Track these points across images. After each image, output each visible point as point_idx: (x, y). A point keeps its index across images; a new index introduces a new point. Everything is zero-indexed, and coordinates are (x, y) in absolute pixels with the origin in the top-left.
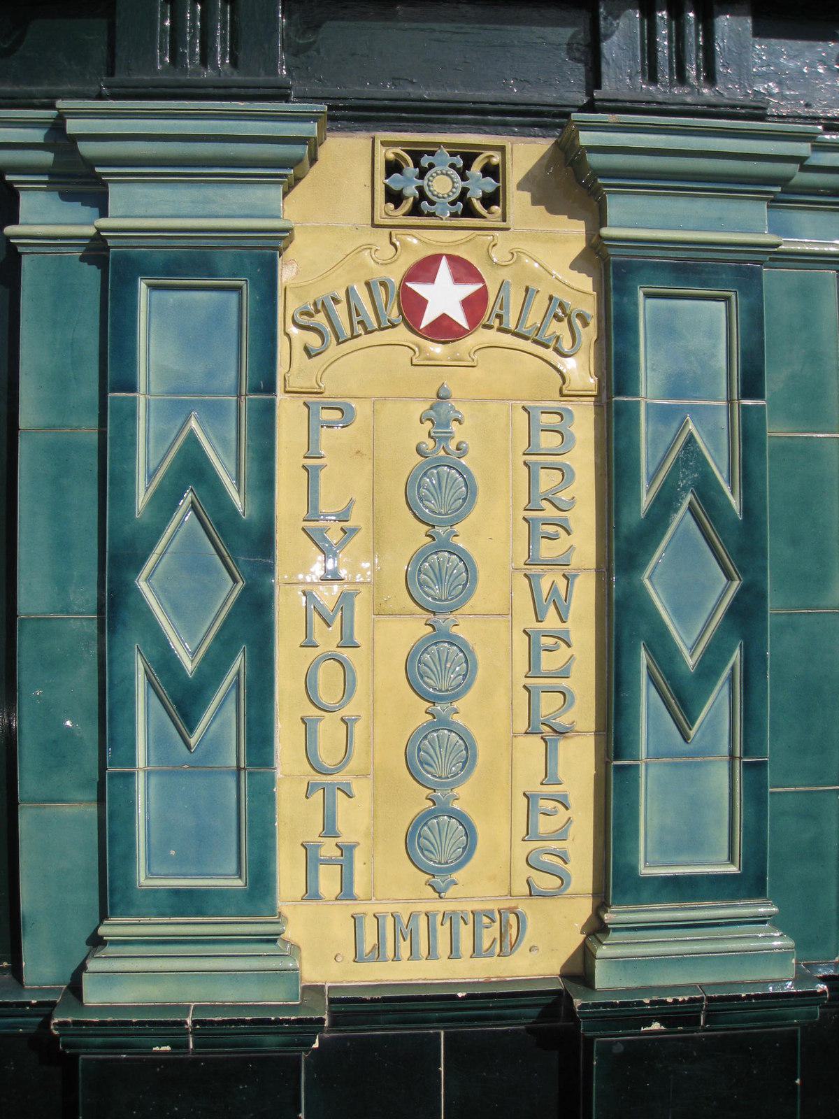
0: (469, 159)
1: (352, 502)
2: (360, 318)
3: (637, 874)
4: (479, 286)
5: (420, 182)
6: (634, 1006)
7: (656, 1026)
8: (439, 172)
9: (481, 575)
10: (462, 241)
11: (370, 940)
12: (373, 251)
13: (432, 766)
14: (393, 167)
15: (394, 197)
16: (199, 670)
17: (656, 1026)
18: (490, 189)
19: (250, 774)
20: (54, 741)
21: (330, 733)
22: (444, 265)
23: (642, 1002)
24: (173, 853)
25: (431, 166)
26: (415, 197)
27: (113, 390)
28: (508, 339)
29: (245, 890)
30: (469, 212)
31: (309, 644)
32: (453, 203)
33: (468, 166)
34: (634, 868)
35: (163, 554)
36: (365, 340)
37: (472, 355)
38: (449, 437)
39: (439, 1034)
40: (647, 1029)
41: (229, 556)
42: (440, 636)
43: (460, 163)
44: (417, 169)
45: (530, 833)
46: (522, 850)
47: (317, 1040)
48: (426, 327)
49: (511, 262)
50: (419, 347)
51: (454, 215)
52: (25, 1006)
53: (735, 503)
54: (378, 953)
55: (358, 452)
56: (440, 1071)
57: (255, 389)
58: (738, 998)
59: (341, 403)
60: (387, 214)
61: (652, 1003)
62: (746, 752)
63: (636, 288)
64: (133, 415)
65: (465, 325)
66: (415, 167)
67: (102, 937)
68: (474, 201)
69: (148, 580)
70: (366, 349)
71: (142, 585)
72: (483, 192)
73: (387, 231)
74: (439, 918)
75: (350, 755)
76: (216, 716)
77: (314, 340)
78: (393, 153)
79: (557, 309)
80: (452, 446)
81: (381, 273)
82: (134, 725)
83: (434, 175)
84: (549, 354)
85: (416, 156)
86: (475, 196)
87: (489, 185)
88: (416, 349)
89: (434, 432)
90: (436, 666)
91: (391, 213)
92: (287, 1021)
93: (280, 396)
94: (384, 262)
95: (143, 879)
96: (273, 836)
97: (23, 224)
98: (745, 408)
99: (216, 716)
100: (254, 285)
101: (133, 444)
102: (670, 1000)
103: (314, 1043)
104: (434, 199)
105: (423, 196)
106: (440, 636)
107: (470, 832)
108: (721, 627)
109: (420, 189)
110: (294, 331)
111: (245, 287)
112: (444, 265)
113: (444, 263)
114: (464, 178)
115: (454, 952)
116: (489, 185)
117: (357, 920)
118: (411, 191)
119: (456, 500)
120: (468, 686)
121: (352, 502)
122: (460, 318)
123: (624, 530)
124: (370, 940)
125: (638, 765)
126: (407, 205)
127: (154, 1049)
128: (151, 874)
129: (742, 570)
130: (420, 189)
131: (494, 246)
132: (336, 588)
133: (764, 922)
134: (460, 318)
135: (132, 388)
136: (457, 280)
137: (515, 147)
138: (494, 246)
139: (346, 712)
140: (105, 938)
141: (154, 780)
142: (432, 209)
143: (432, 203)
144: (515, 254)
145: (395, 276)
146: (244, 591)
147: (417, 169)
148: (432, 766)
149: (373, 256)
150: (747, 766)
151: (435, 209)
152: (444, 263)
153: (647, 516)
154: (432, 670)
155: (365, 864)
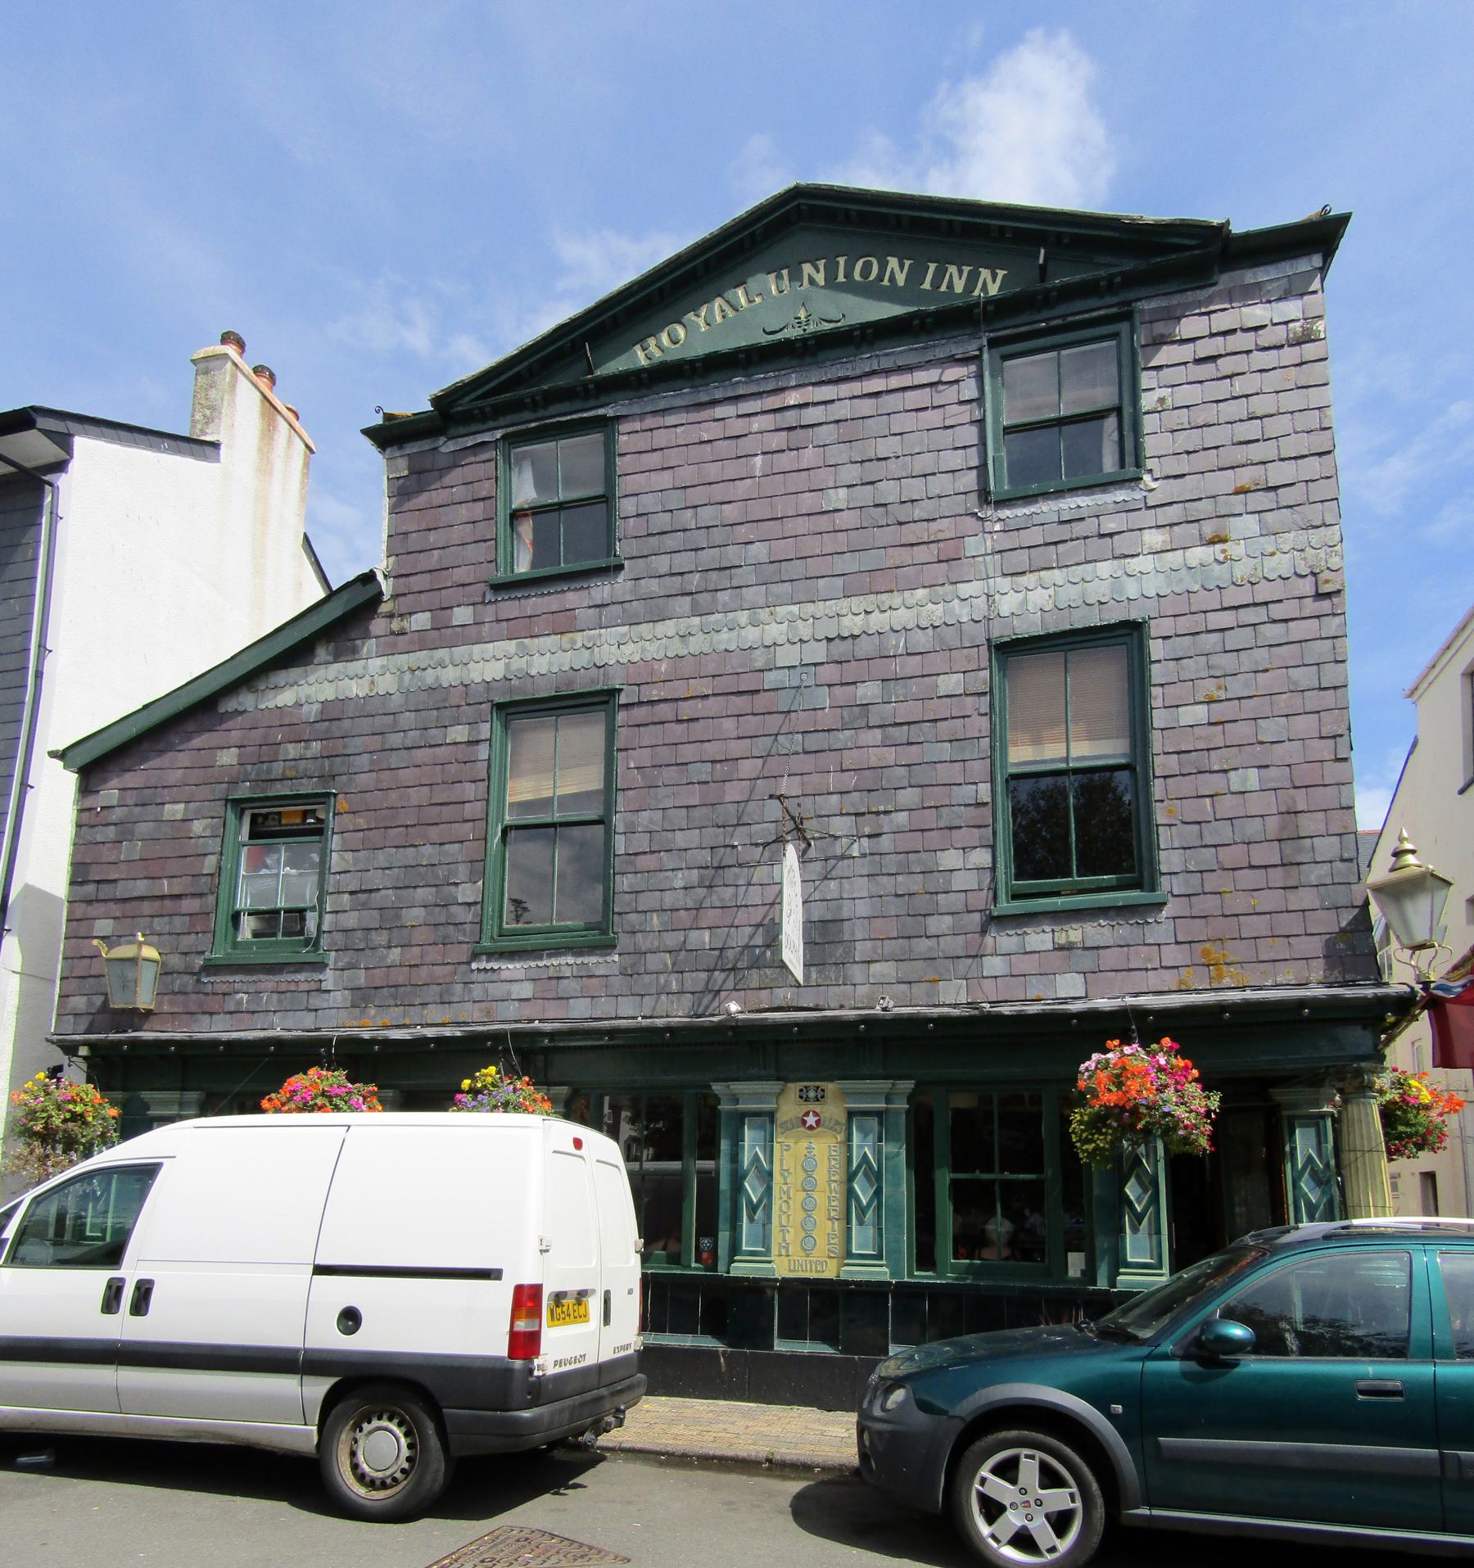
0: (818, 1088)
14: (801, 1090)
15: (801, 1097)
21: (784, 1217)
30: (818, 1100)
31: (781, 1198)
46: (827, 1247)
54: (794, 1271)
71: (746, 1184)
79: (837, 1123)
95: (744, 1248)
115: (811, 1271)
117: (790, 1261)
122: (814, 1125)
134: (814, 1125)
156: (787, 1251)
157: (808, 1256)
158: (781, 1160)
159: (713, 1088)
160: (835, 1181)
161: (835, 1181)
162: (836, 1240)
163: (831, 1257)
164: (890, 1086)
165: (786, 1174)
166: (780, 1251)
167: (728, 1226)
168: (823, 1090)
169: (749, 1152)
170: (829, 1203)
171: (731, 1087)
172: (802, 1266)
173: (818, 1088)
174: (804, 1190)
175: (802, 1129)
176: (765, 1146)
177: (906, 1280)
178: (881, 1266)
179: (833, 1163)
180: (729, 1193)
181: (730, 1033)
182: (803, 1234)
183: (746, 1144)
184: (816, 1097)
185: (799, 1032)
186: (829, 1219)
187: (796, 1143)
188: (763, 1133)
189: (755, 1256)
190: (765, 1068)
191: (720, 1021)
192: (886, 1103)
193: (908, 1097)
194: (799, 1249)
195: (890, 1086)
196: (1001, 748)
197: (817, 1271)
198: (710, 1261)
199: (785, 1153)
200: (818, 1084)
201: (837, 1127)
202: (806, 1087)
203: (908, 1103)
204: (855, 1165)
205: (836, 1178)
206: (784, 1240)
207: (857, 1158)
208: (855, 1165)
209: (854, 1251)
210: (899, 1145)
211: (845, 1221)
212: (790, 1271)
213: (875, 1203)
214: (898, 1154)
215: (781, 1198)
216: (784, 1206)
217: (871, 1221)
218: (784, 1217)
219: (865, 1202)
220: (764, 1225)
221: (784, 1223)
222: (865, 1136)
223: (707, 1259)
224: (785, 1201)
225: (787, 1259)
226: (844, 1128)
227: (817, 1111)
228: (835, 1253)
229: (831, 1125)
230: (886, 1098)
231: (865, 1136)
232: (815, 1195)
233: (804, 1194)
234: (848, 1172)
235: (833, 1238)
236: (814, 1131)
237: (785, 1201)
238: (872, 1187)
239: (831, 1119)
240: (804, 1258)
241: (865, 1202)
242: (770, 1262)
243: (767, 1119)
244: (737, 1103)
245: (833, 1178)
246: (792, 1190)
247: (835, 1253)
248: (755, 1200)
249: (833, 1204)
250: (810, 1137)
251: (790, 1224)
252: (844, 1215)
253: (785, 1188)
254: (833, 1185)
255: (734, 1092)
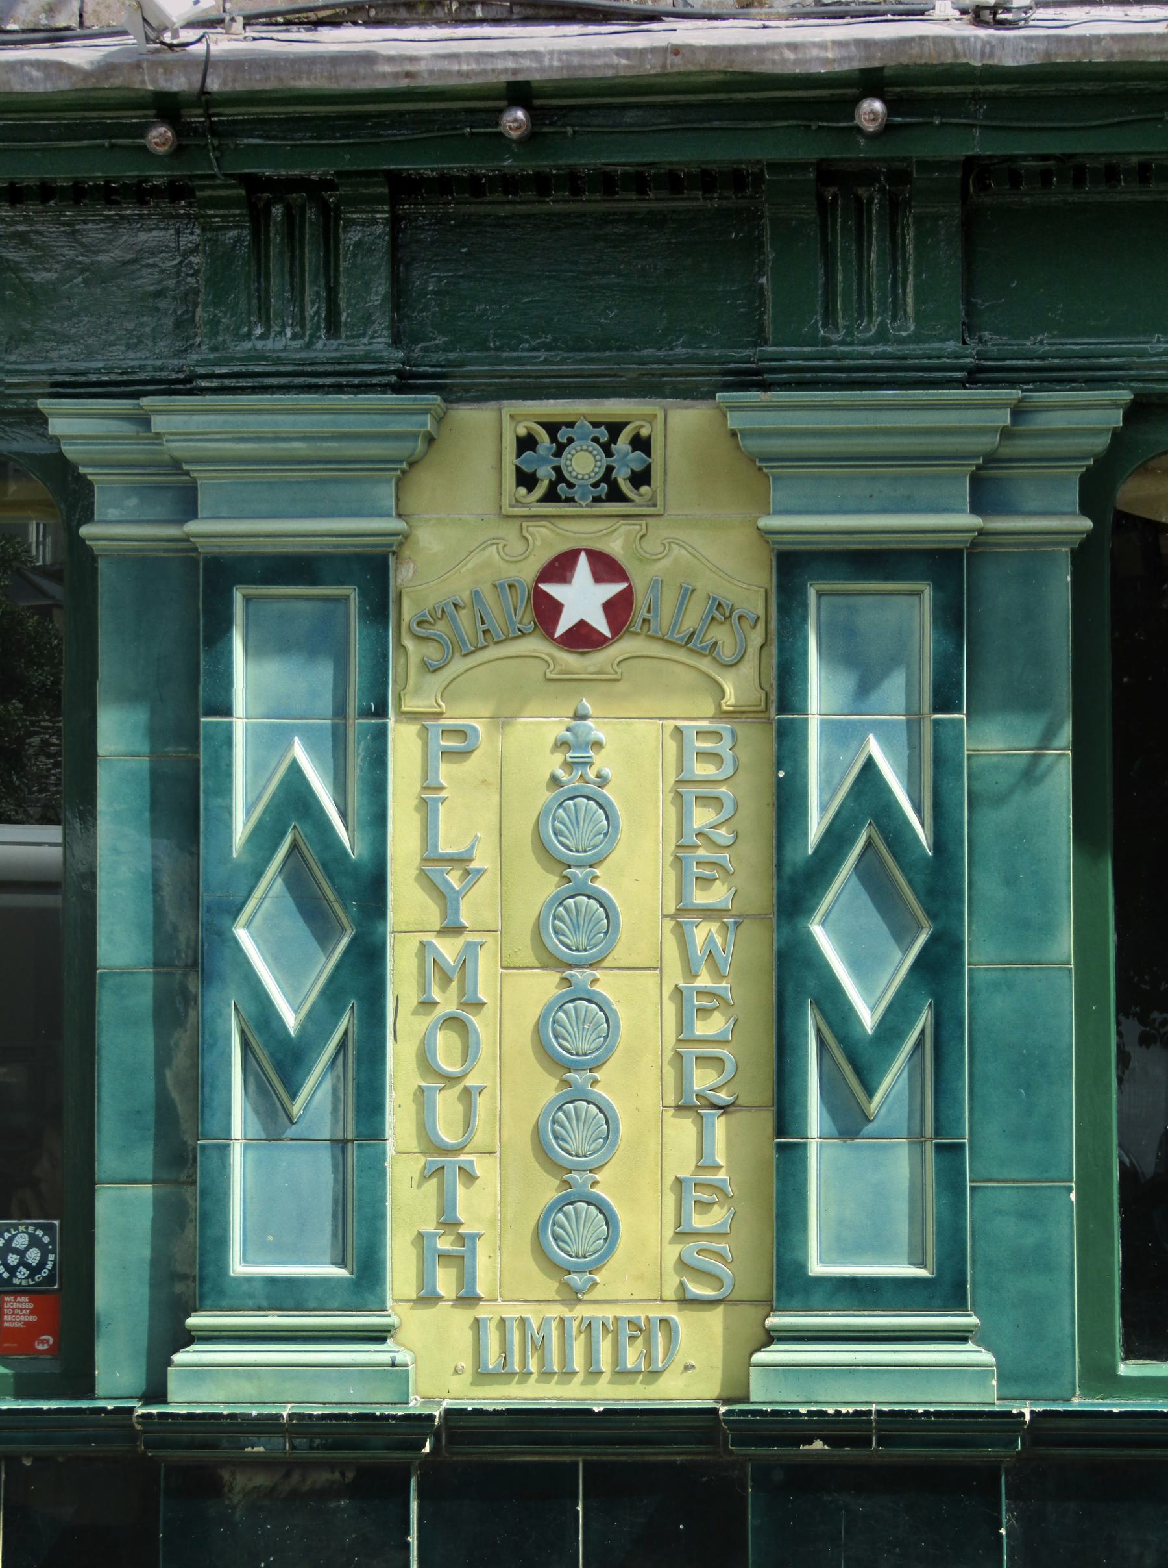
0: (615, 429)
1: (476, 839)
2: (485, 627)
3: (806, 1273)
4: (624, 585)
5: (556, 461)
6: (788, 1416)
7: (818, 1445)
8: (579, 448)
9: (624, 919)
10: (604, 532)
11: (493, 1358)
12: (500, 546)
13: (568, 1143)
14: (526, 444)
15: (526, 480)
16: (303, 1028)
17: (818, 1445)
18: (638, 468)
19: (359, 1146)
20: (138, 1112)
21: (446, 1104)
22: (583, 561)
23: (798, 1411)
24: (270, 1238)
25: (571, 440)
26: (550, 480)
27: (207, 714)
28: (656, 649)
29: (352, 1279)
30: (616, 495)
31: (427, 1005)
32: (596, 485)
33: (614, 439)
34: (802, 1267)
35: (262, 900)
36: (493, 652)
37: (615, 666)
38: (586, 763)
39: (576, 1464)
40: (807, 1447)
41: (328, 901)
42: (575, 994)
43: (605, 438)
44: (554, 445)
45: (682, 1234)
46: (672, 1252)
47: (428, 1444)
48: (562, 636)
49: (664, 554)
50: (553, 658)
51: (597, 499)
52: (942, 124)
53: (922, 834)
54: (504, 1375)
55: (484, 782)
56: (578, 1511)
57: (365, 713)
58: (914, 1413)
59: (464, 725)
60: (517, 501)
61: (810, 1413)
62: (937, 1133)
63: (806, 585)
64: (229, 742)
65: (607, 633)
66: (552, 442)
67: (190, 1331)
68: (620, 481)
69: (823, 923)
70: (493, 663)
71: (242, 935)
72: (649, 437)
73: (518, 522)
74: (575, 1324)
75: (473, 1128)
76: (321, 1082)
77: (432, 652)
78: (526, 427)
79: (720, 612)
80: (591, 774)
81: (511, 572)
82: (230, 1091)
83: (569, 456)
84: (705, 664)
85: (552, 428)
86: (622, 477)
87: (636, 460)
88: (551, 663)
89: (571, 758)
90: (571, 1025)
91: (523, 500)
92: (394, 1417)
93: (391, 722)
94: (512, 559)
95: (238, 1267)
96: (383, 1217)
97: (100, 522)
98: (936, 723)
99: (321, 1082)
100: (363, 594)
101: (229, 775)
102: (831, 1411)
103: (424, 1446)
104: (572, 480)
105: (561, 478)
106: (575, 994)
107: (610, 1220)
108: (905, 983)
109: (557, 469)
110: (409, 643)
111: (352, 596)
112: (583, 561)
113: (583, 559)
114: (609, 454)
115: (594, 1374)
116: (636, 460)
117: (477, 1325)
118: (545, 473)
119: (595, 836)
120: (610, 1051)
121: (476, 839)
122: (602, 625)
123: (788, 870)
124: (493, 1358)
125: (805, 1145)
126: (541, 489)
127: (246, 1450)
128: (245, 1260)
129: (932, 916)
130: (557, 469)
131: (642, 537)
132: (459, 942)
133: (964, 1340)
134: (602, 625)
135: (228, 712)
136: (598, 579)
137: (671, 413)
138: (642, 537)
139: (469, 1082)
140: (193, 1333)
141: (251, 1154)
142: (570, 492)
143: (571, 485)
144: (667, 545)
145: (528, 572)
146: (353, 941)
147: (554, 445)
148: (568, 1143)
149: (501, 552)
150: (939, 1148)
151: (576, 493)
152: (583, 559)
153: (816, 852)
154: (567, 1031)
155: (490, 1257)
156: (466, 1279)
157: (573, 1297)
158: (427, 808)
159: (56, 426)
160: (708, 913)
161: (708, 913)
162: (716, 1217)
163: (686, 1301)
164: (1004, 418)
165: (454, 878)
166: (425, 1279)
167: (144, 1157)
168: (641, 444)
169: (257, 768)
170: (682, 1024)
171: (159, 423)
172: (541, 1347)
173: (615, 429)
174: (550, 961)
175: (535, 645)
176: (339, 738)
177: (1078, 1403)
178: (958, 1336)
179: (702, 817)
180: (147, 979)
181: (160, 136)
182: (549, 1190)
183: (239, 726)
184: (608, 476)
185: (532, 139)
186: (682, 1108)
187: (501, 721)
188: (324, 673)
189: (300, 1306)
190: (333, 326)
191: (107, 68)
192: (976, 509)
193: (1085, 480)
194: (528, 1264)
195: (1004, 418)
196: (906, 85)
197: (621, 1374)
198: (45, 1342)
199: (445, 771)
200: (613, 408)
201: (720, 634)
202: (552, 428)
203: (1086, 509)
204: (816, 826)
205: (717, 895)
206: (449, 1223)
207: (828, 786)
208: (816, 826)
209: (816, 1268)
210: (1037, 726)
211: (767, 1119)
212: (482, 1375)
213: (924, 1019)
214: (1031, 773)
215: (427, 1005)
216: (446, 1047)
217: (901, 1114)
218: (446, 1104)
219: (868, 1018)
220: (340, 1145)
221: (447, 1135)
222: (865, 688)
223: (30, 1332)
224: (452, 1021)
225: (463, 1318)
226: (756, 638)
227: (615, 547)
228: (712, 1277)
229: (691, 621)
230: (977, 482)
231: (865, 688)
232: (606, 984)
233: (547, 984)
234: (780, 865)
235: (703, 1206)
236: (640, 600)
237: (452, 1021)
238: (901, 934)
239: (687, 593)
240: (557, 1311)
241: (868, 1018)
242: (378, 1336)
243: (351, 592)
244: (190, 511)
245: (700, 898)
246: (486, 966)
247: (712, 1277)
248: (291, 1020)
249: (702, 1028)
250: (569, 682)
251: (480, 1137)
252: (760, 1090)
253: (449, 950)
254: (702, 933)
255: (178, 448)
